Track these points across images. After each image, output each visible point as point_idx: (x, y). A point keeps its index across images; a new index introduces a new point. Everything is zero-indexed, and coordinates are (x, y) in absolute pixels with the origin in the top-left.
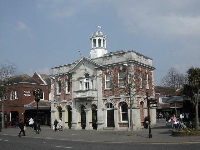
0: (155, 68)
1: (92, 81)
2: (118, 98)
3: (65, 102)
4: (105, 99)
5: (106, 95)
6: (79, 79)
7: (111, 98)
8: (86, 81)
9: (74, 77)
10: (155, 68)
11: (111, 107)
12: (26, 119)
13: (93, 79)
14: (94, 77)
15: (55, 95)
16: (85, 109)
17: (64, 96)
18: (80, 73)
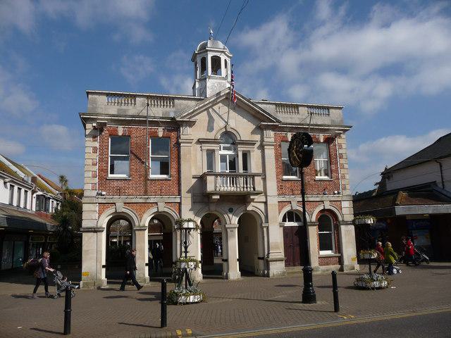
2: (318, 199)
4: (284, 199)
9: (187, 133)
10: (351, 127)
15: (101, 178)
17: (146, 185)
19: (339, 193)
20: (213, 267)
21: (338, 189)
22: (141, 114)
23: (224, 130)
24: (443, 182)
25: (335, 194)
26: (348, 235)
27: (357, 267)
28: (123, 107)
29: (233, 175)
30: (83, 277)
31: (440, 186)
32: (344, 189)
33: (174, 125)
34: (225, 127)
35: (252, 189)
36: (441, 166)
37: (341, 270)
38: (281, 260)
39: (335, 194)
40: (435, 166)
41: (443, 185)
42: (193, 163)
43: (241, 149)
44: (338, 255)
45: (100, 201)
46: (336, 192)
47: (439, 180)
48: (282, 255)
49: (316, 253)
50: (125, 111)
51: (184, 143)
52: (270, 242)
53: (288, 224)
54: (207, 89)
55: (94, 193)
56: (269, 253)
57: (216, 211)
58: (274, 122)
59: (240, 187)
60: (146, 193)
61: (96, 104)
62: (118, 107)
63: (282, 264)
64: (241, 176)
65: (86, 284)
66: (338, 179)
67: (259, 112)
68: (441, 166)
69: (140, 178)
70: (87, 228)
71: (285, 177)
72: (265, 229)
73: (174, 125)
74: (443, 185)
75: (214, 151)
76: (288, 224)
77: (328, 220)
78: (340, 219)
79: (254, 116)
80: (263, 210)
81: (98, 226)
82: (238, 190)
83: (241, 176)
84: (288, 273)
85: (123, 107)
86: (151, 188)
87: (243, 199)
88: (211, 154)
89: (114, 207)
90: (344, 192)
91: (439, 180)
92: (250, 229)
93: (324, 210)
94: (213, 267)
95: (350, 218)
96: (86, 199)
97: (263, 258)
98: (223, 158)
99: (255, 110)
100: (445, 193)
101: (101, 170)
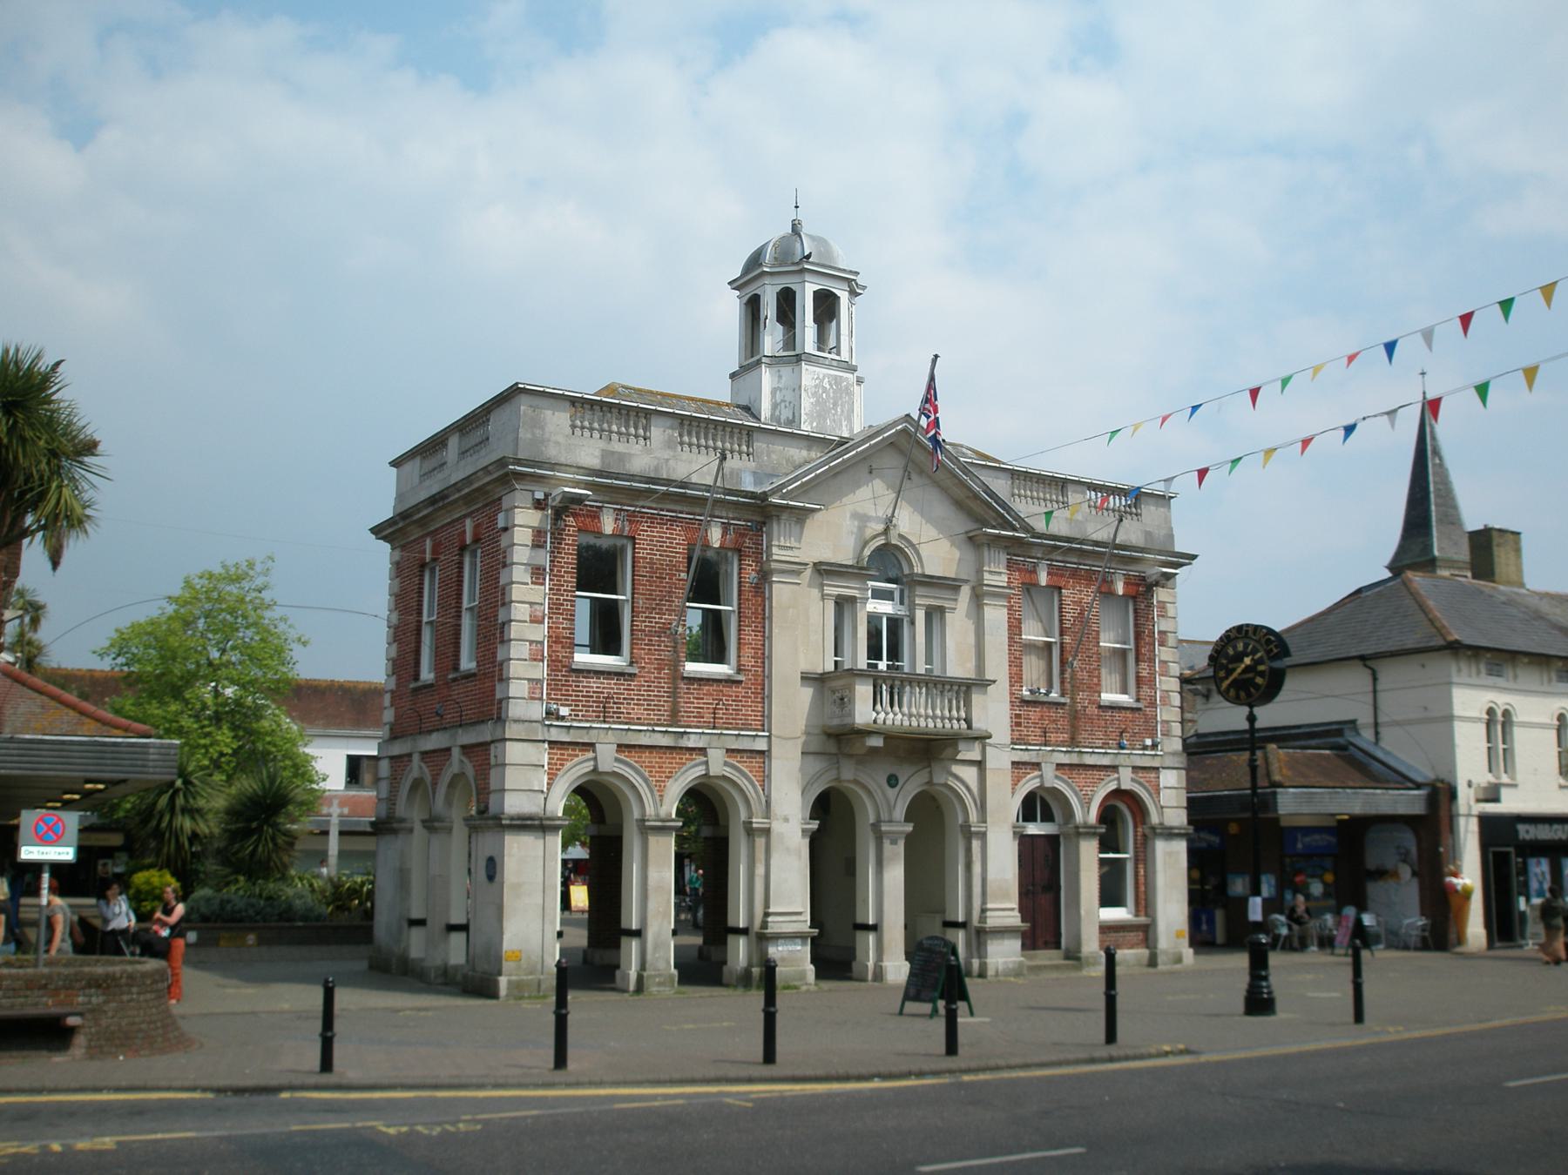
0: (1194, 557)
1: (935, 615)
2: (1106, 761)
3: (691, 742)
4: (1025, 757)
5: (1034, 734)
6: (824, 571)
7: (1065, 759)
8: (885, 608)
9: (786, 547)
10: (1194, 557)
11: (1048, 817)
12: (47, 868)
13: (946, 604)
14: (949, 585)
15: (555, 665)
16: (1456, 875)
17: (674, 694)
18: (832, 534)
19: (1154, 746)
20: (835, 957)
21: (1153, 735)
22: (694, 479)
23: (881, 541)
24: (1376, 724)
25: (1145, 748)
26: (1171, 866)
27: (1188, 953)
28: (618, 446)
29: (894, 679)
30: (506, 966)
31: (1368, 734)
32: (1166, 734)
33: (759, 515)
34: (886, 531)
35: (964, 725)
36: (1375, 679)
37: (1153, 962)
38: (1524, 725)
39: (1145, 748)
40: (1357, 679)
41: (1377, 733)
42: (803, 631)
43: (923, 600)
44: (1142, 919)
45: (555, 735)
46: (1148, 742)
47: (1364, 717)
48: (1014, 919)
49: (1094, 915)
50: (622, 457)
51: (783, 572)
52: (990, 877)
53: (1033, 829)
54: (803, 394)
55: (537, 711)
56: (984, 911)
57: (856, 782)
58: (1015, 529)
59: (917, 713)
60: (674, 718)
61: (542, 428)
62: (602, 444)
63: (1016, 944)
64: (860, 674)
65: (517, 988)
66: (1153, 704)
67: (976, 496)
68: (1375, 679)
69: (660, 669)
70: (520, 817)
71: (692, 668)
72: (976, 844)
73: (759, 515)
74: (1377, 733)
75: (853, 600)
76: (1033, 829)
77: (1121, 816)
78: (1154, 819)
79: (959, 504)
80: (975, 789)
81: (548, 814)
82: (931, 725)
83: (860, 674)
84: (1032, 969)
85: (618, 446)
86: (691, 702)
87: (927, 749)
88: (844, 605)
89: (591, 755)
90: (1166, 741)
91: (1364, 717)
92: (934, 831)
93: (1118, 793)
94: (835, 957)
95: (1177, 817)
96: (515, 727)
97: (963, 925)
98: (873, 619)
99: (970, 489)
100: (1380, 755)
101: (555, 639)
